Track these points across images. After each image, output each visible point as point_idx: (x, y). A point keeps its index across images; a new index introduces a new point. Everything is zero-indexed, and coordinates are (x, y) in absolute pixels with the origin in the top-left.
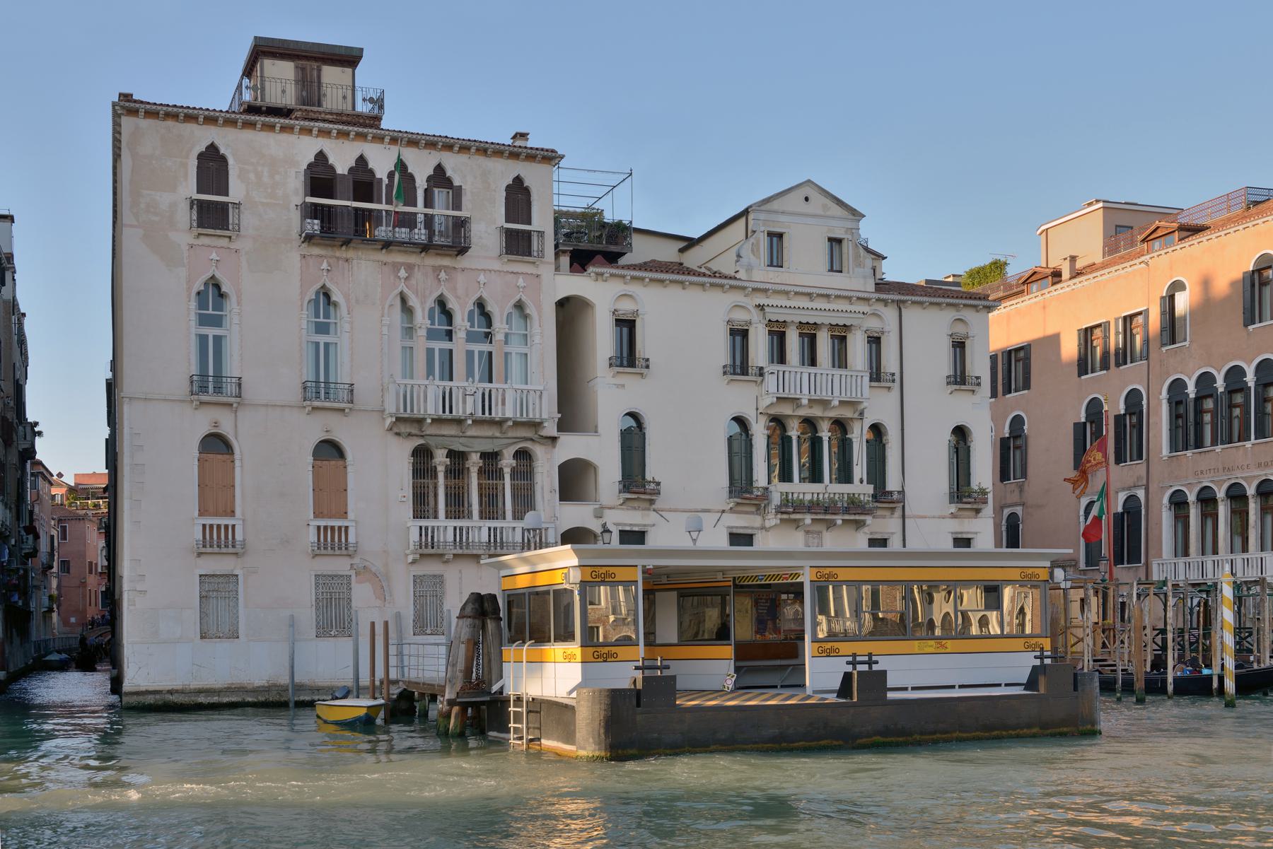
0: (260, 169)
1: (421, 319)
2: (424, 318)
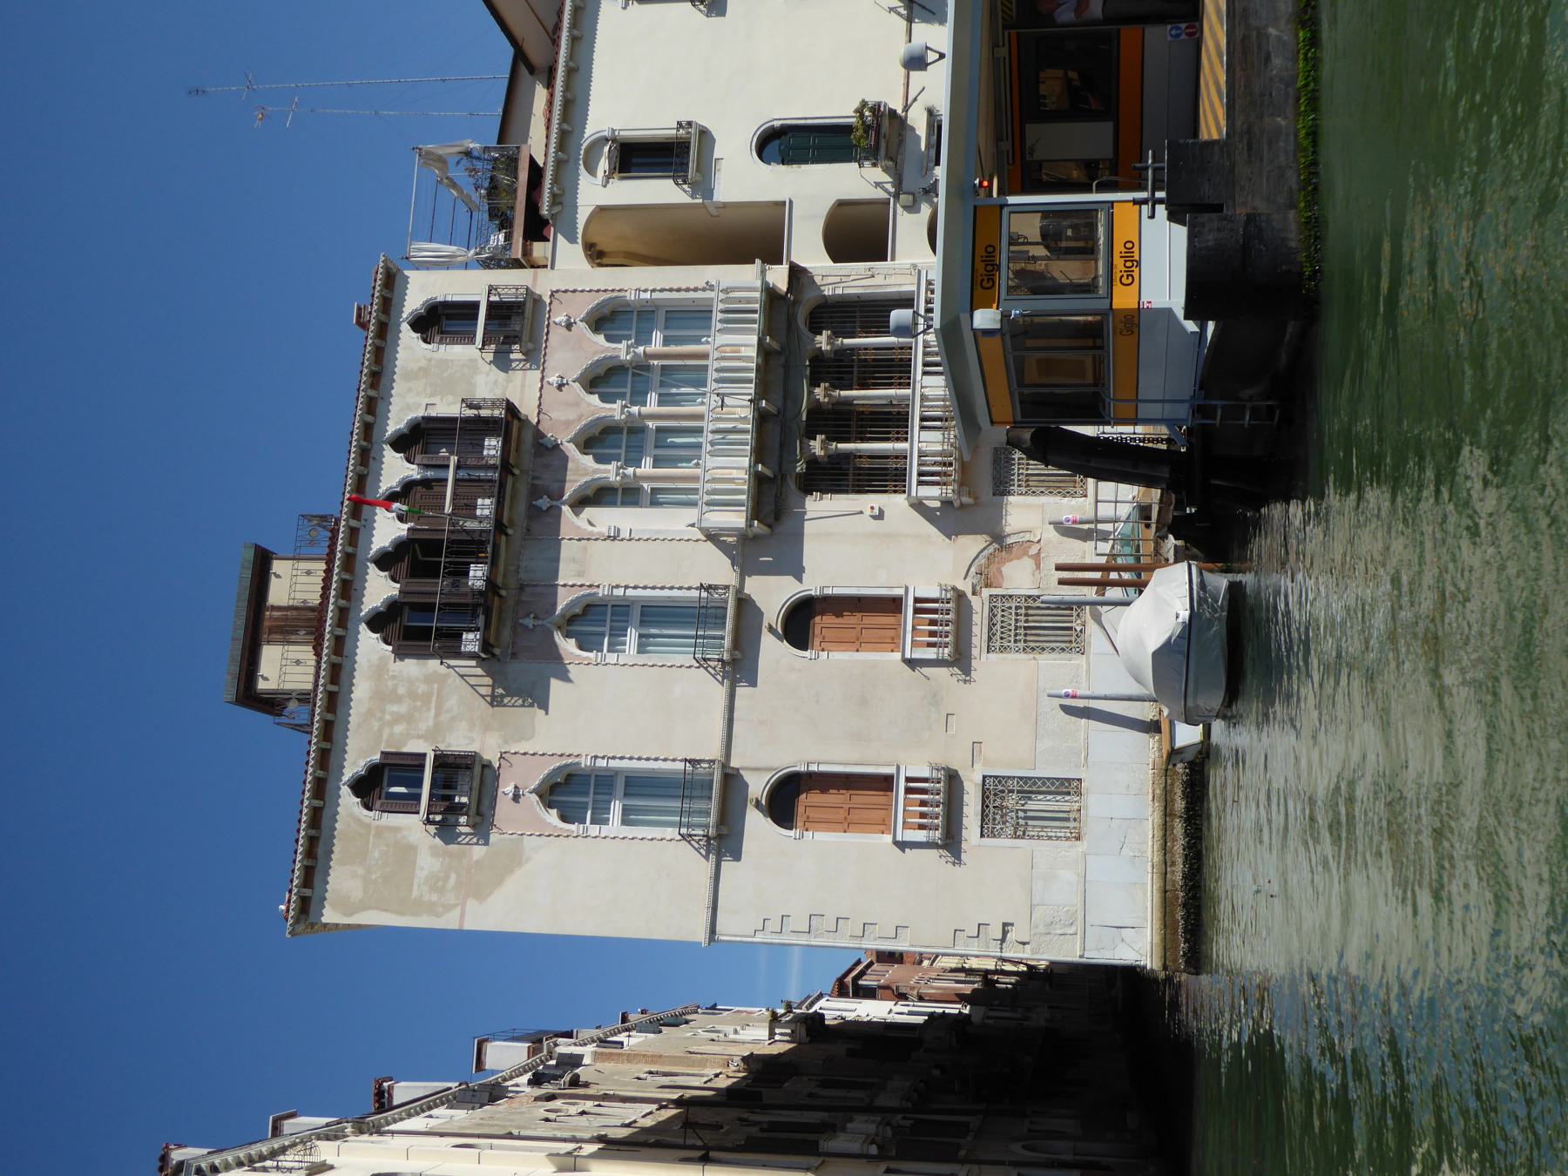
0: (388, 717)
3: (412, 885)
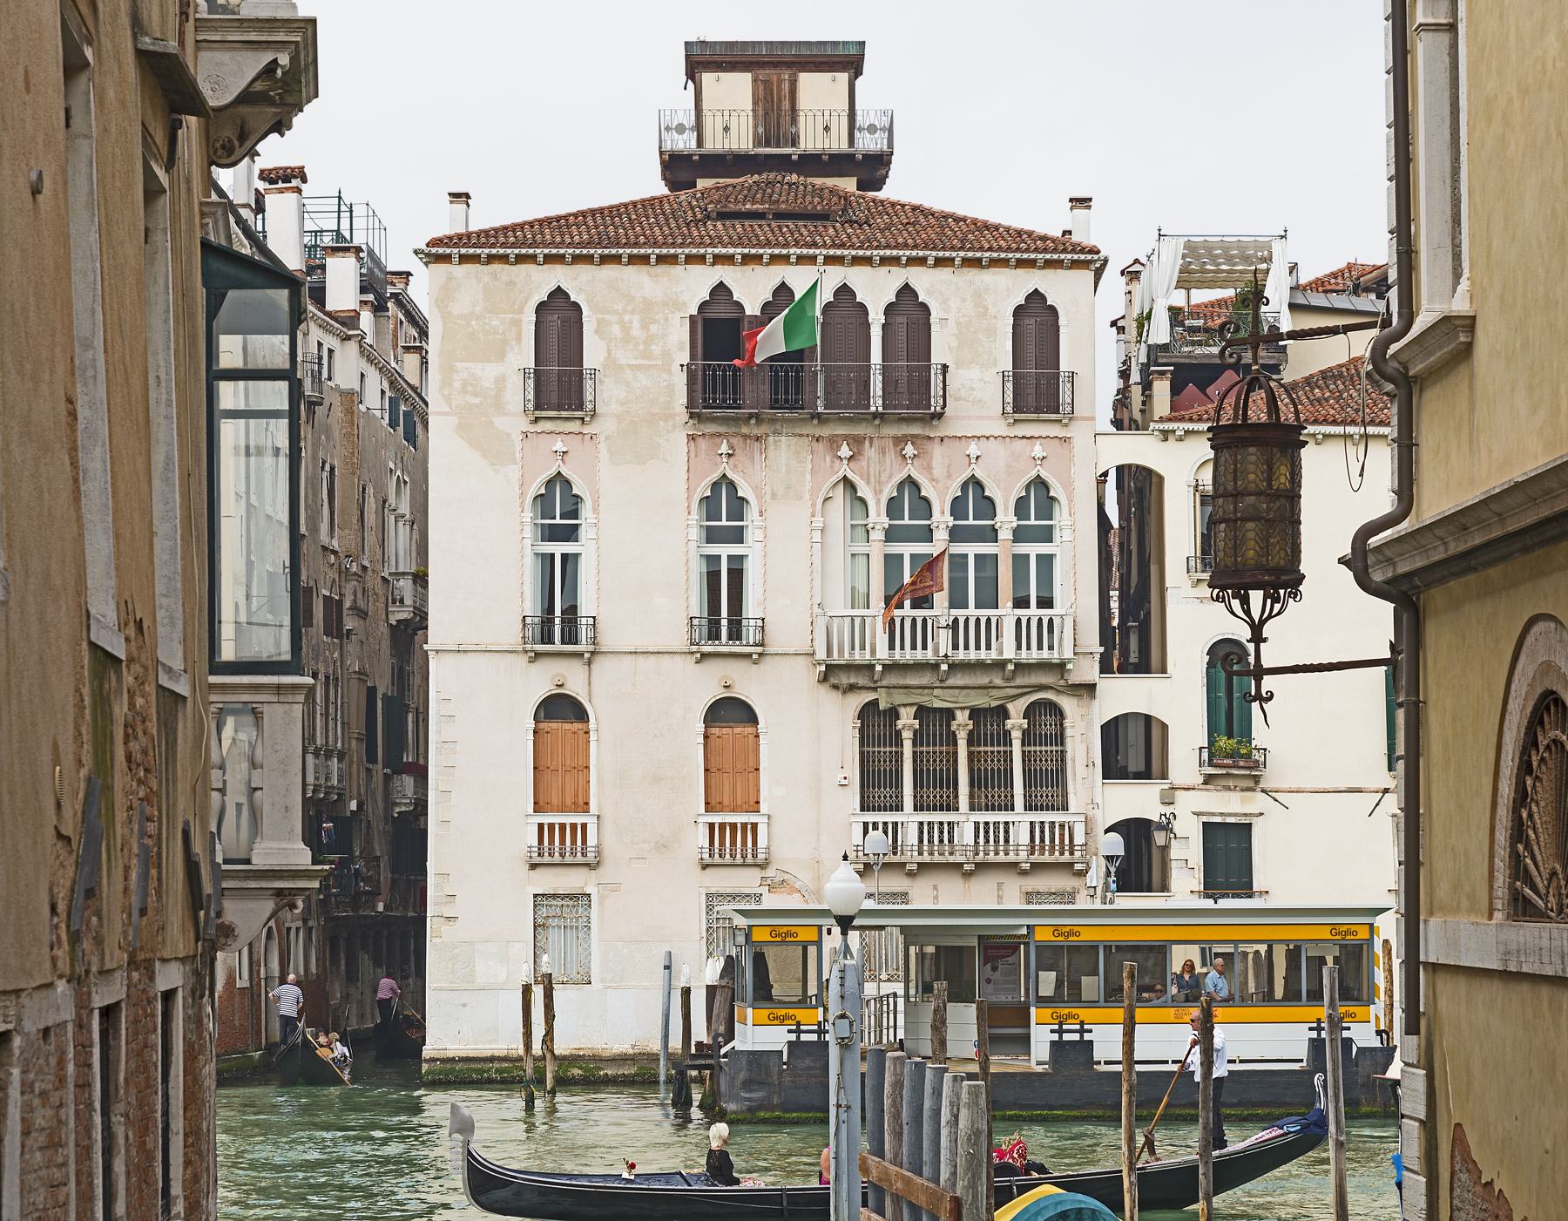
0: (627, 318)
2: (879, 515)
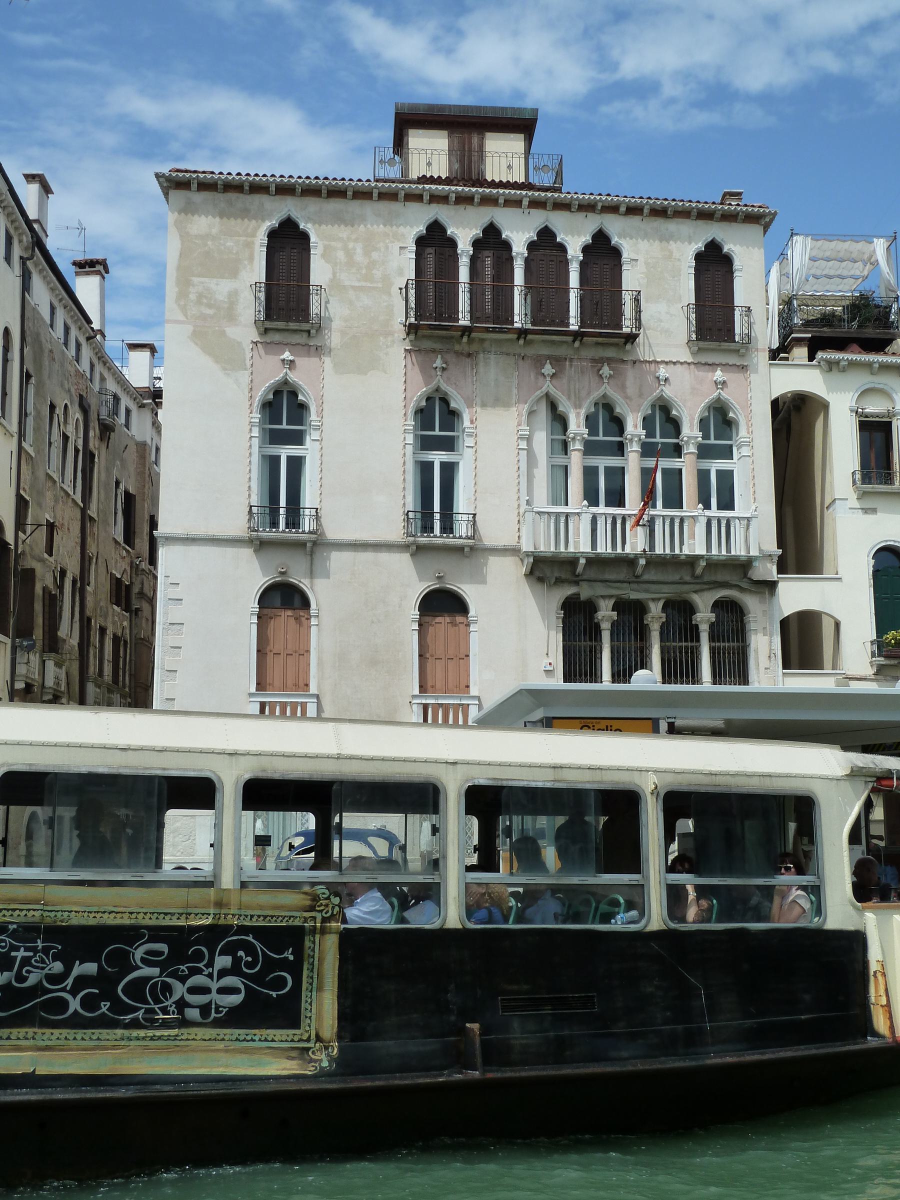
0: (351, 245)
1: (577, 425)
3: (203, 277)
